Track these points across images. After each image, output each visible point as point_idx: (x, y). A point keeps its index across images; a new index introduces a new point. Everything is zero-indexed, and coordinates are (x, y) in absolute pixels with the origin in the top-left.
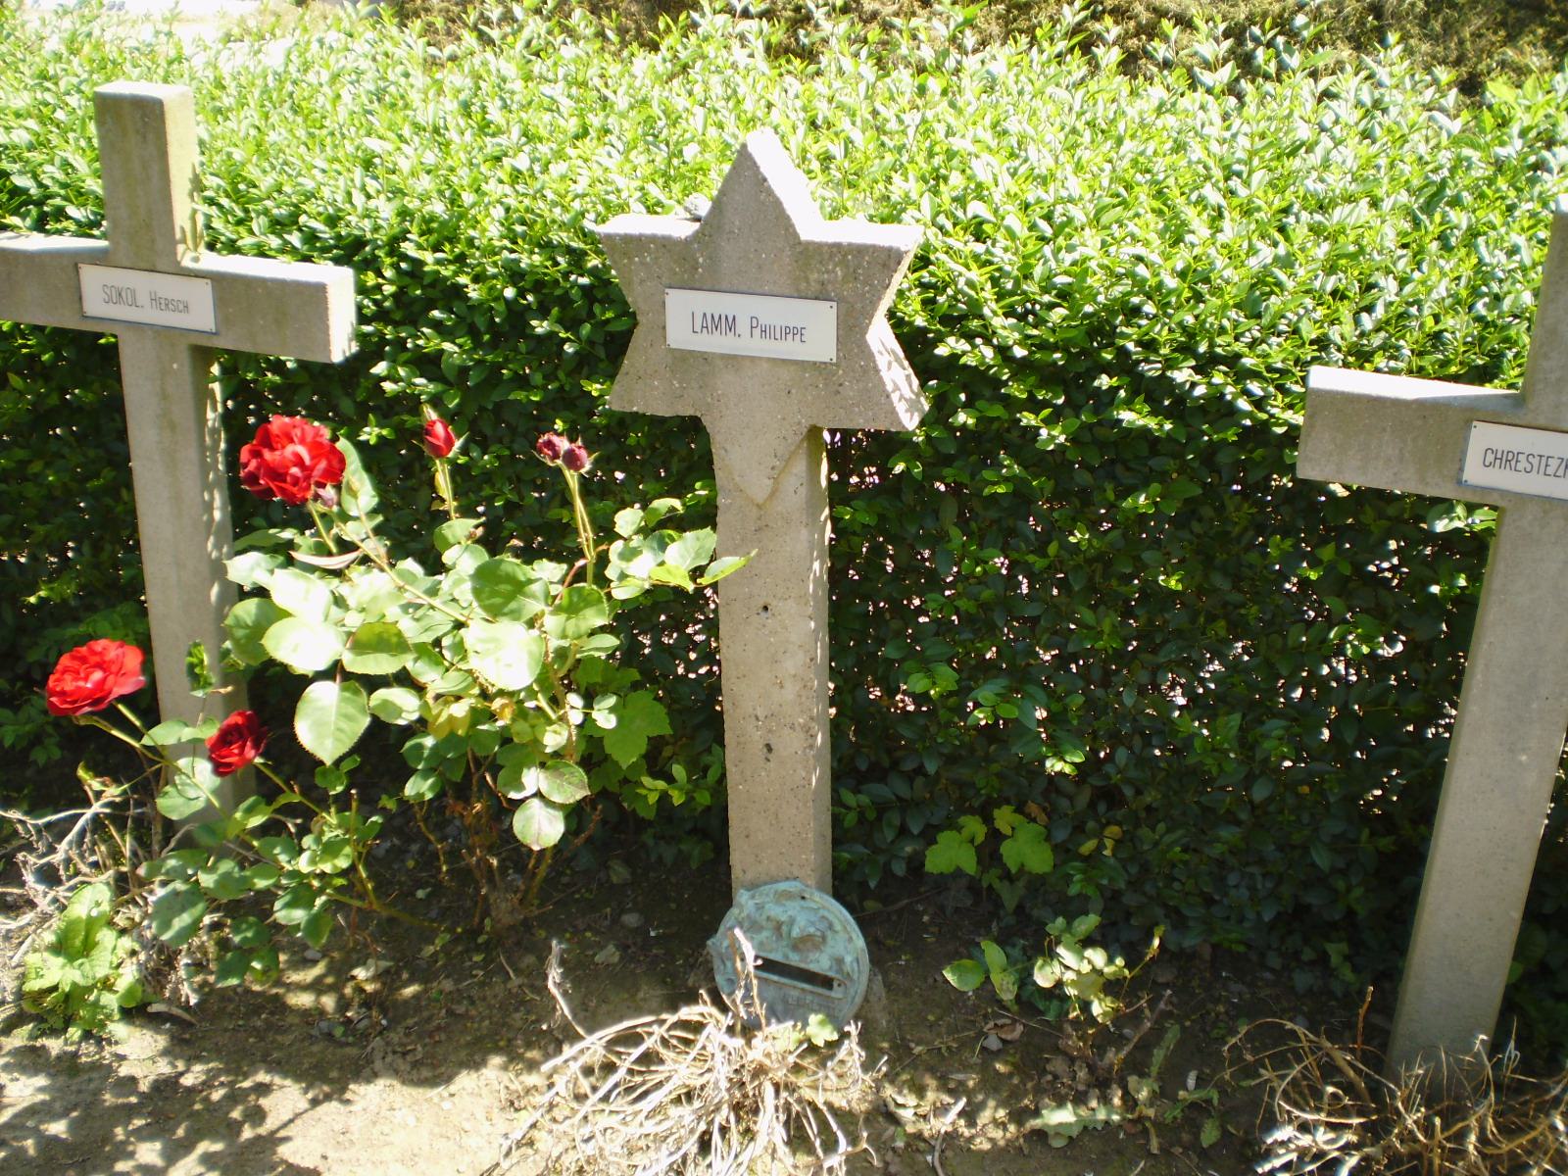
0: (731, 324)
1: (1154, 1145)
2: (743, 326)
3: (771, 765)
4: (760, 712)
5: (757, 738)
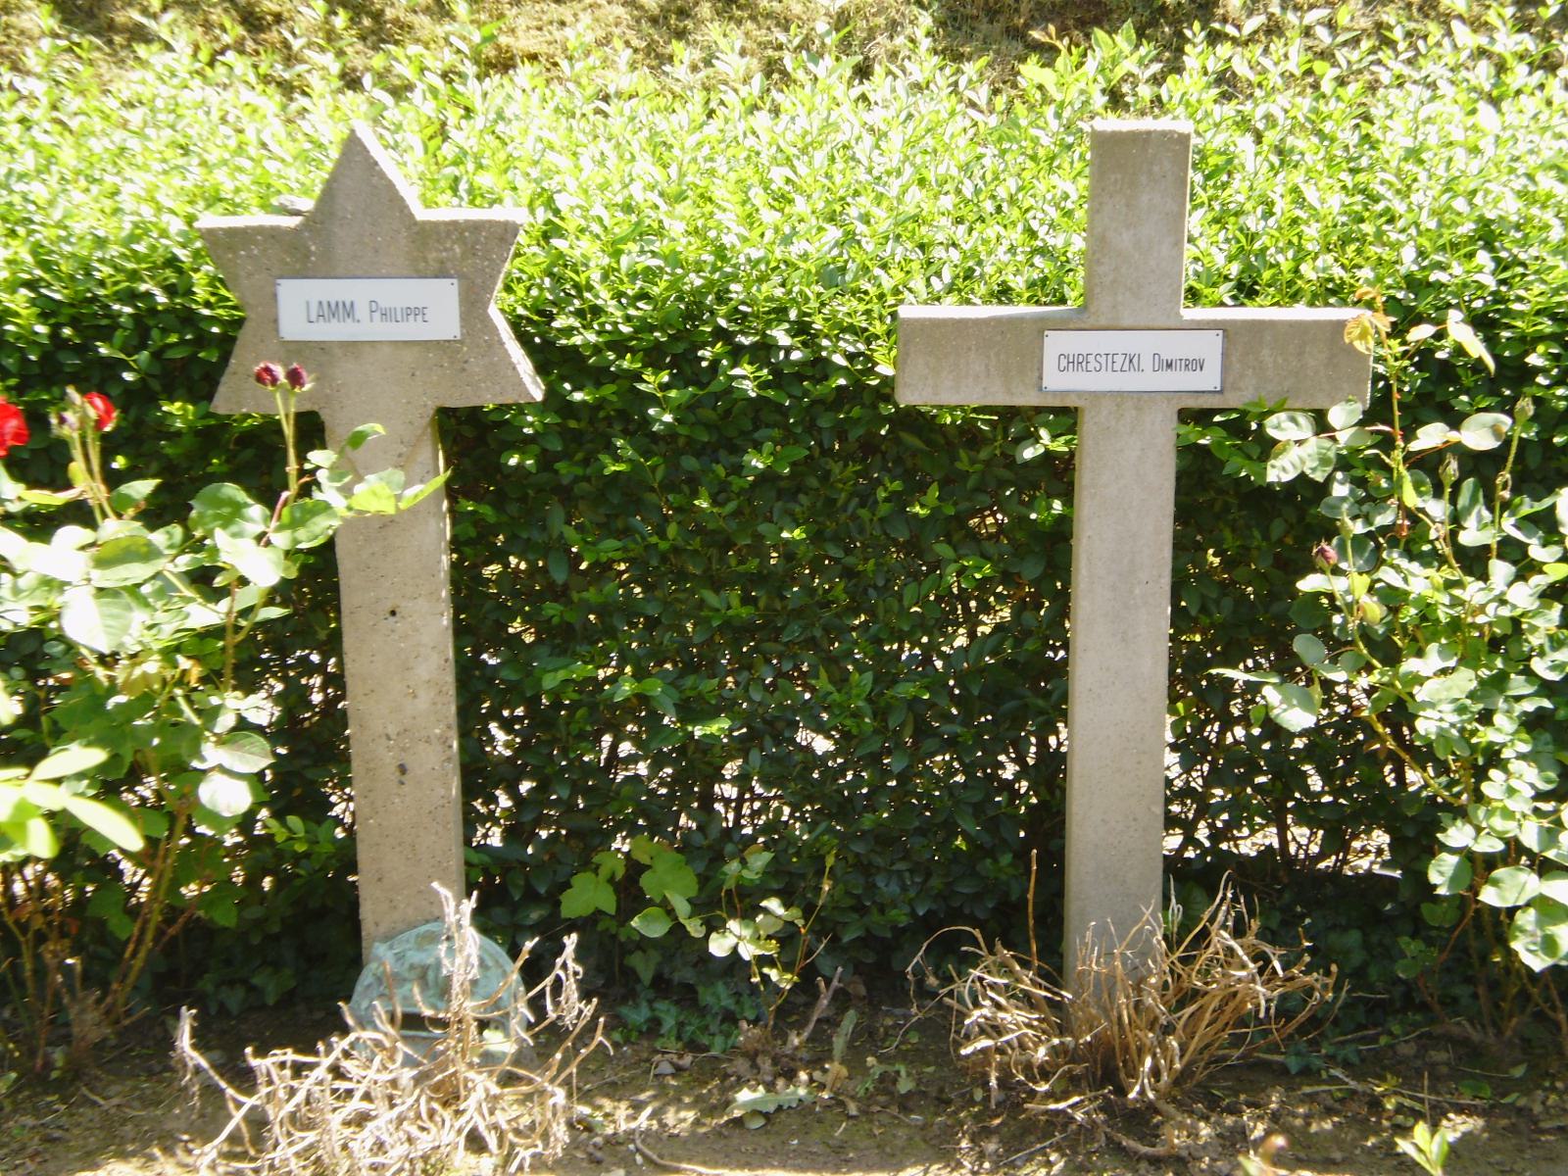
0: (347, 311)
1: (853, 1109)
2: (362, 311)
3: (406, 789)
4: (392, 730)
5: (389, 759)
